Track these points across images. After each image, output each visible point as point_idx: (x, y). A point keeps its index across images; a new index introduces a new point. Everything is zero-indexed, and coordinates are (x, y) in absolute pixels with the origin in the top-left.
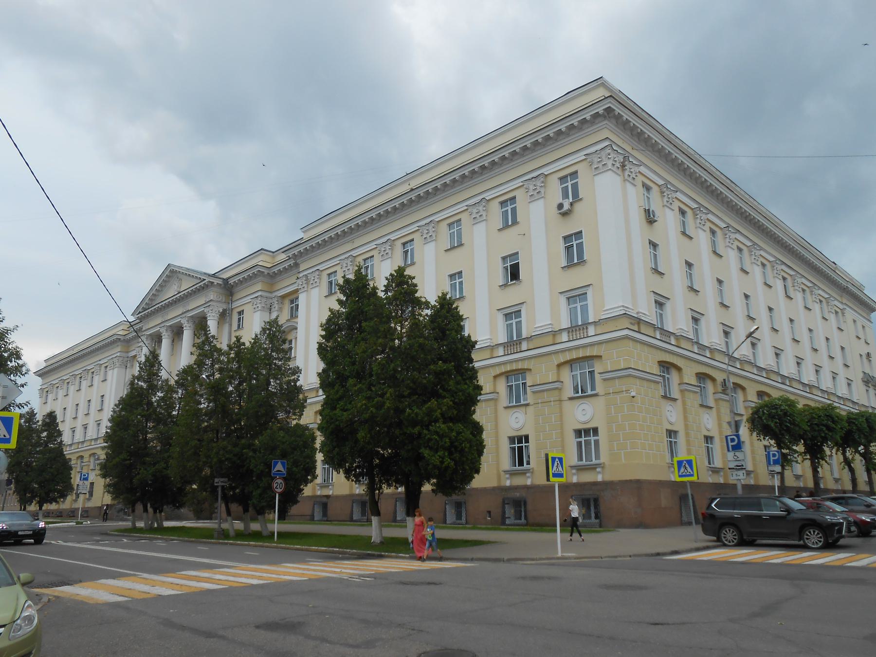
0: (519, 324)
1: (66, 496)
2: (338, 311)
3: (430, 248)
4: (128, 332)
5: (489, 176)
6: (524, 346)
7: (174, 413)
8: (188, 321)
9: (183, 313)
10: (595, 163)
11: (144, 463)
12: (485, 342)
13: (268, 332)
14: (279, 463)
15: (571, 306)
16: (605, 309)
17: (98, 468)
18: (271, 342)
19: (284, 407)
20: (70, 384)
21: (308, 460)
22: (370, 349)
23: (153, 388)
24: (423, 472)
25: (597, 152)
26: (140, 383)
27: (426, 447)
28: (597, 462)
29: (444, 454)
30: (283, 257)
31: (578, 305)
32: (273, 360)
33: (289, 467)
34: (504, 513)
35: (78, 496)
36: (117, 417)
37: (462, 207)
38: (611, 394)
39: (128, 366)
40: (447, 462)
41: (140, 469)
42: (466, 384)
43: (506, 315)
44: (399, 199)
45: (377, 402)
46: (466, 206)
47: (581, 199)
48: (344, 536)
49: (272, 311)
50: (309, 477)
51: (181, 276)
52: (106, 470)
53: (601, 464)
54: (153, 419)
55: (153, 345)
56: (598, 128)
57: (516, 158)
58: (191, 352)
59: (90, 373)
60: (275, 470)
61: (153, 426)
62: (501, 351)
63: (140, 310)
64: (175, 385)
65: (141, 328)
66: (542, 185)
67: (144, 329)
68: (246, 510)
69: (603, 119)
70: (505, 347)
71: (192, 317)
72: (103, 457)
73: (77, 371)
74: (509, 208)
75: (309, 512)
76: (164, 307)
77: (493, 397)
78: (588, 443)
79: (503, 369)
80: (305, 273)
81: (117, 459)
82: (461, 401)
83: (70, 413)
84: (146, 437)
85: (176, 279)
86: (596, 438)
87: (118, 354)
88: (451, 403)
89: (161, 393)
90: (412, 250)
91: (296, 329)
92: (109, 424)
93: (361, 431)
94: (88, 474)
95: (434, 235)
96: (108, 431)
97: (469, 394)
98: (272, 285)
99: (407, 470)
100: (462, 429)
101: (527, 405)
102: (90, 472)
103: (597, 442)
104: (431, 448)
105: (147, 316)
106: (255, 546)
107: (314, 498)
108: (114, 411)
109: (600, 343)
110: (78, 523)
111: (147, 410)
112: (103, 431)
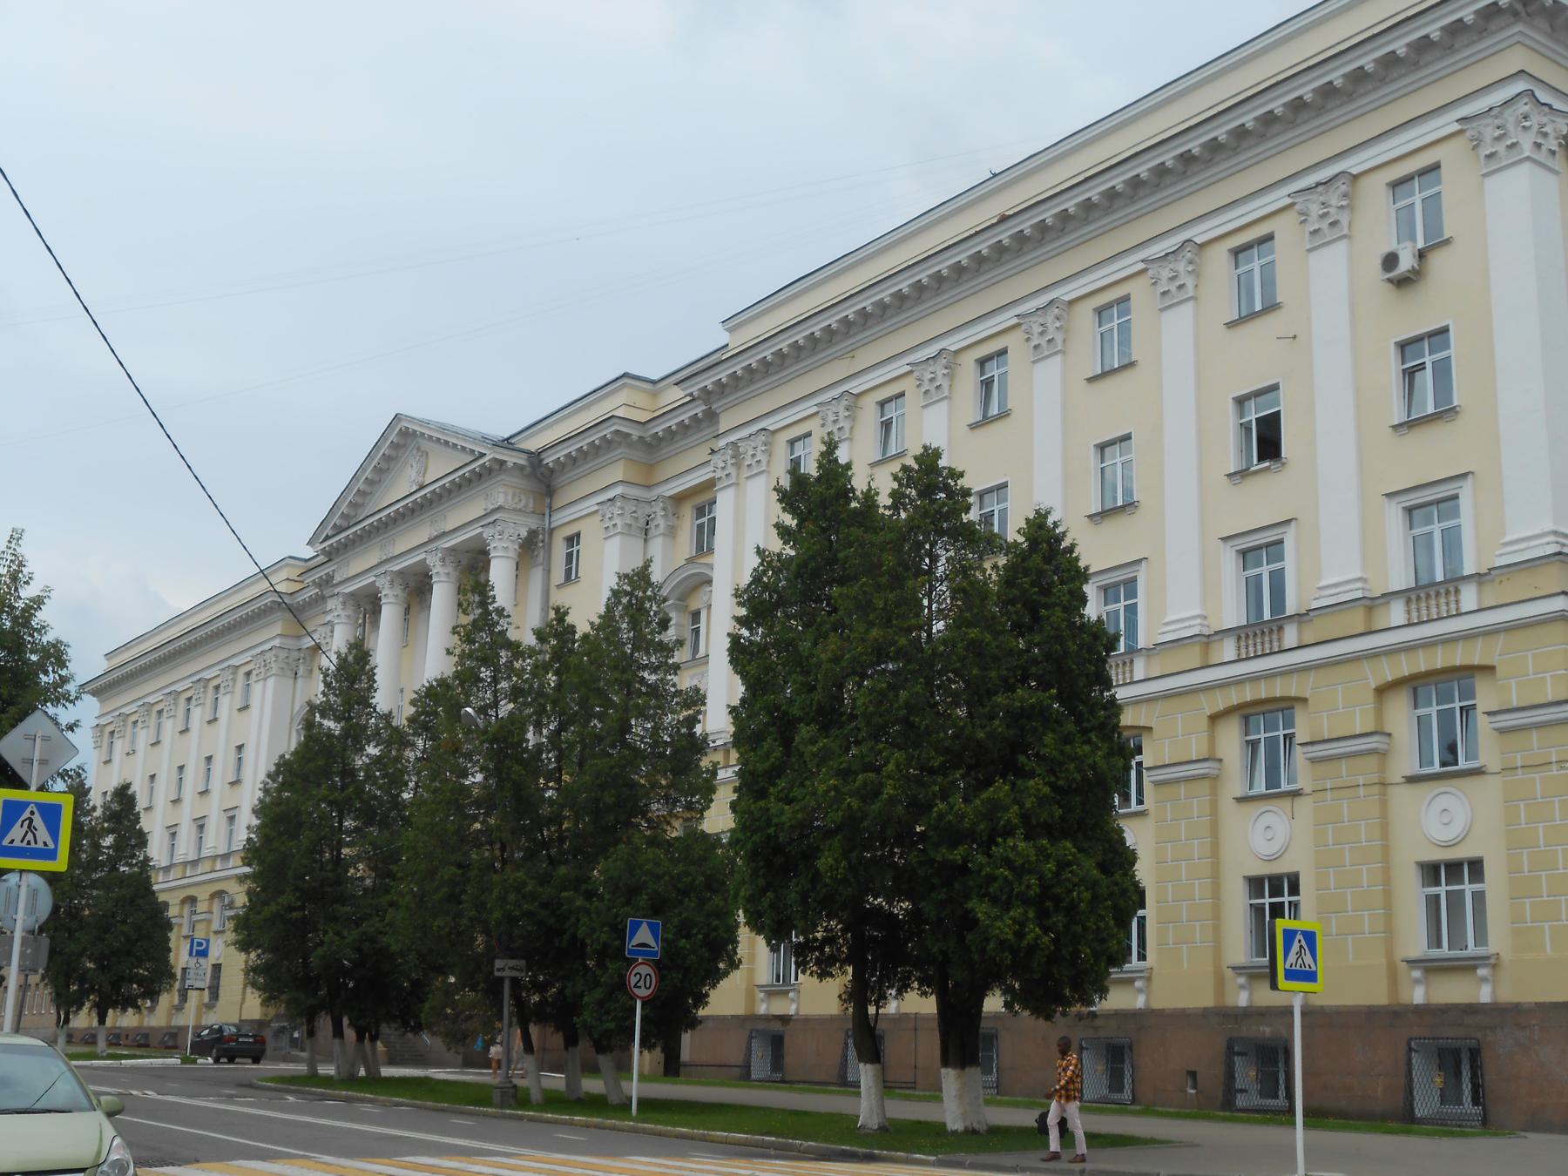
0: (1278, 580)
1: (158, 993)
2: (779, 555)
3: (1049, 372)
4: (299, 586)
5: (879, 331)
6: (1290, 636)
7: (405, 796)
8: (443, 560)
9: (431, 541)
10: (1164, 280)
11: (335, 918)
12: (1187, 624)
13: (625, 600)
14: (644, 925)
15: (1417, 531)
16: (1507, 539)
17: (230, 925)
18: (634, 625)
19: (661, 787)
20: (165, 714)
21: (715, 923)
22: (849, 652)
23: (355, 736)
24: (976, 957)
25: (1494, 112)
26: (326, 722)
27: (981, 896)
28: (1481, 951)
29: (1026, 913)
30: (675, 395)
31: (1436, 529)
32: (639, 668)
33: (670, 936)
34: (1230, 1076)
35: (184, 996)
36: (272, 803)
37: (1132, 263)
38: (1519, 770)
39: (300, 673)
40: (1033, 935)
41: (326, 932)
42: (1089, 742)
43: (1244, 553)
44: (890, 282)
45: (865, 784)
46: (1289, 196)
47: (1447, 242)
48: (805, 1113)
49: (651, 534)
50: (721, 965)
51: (424, 444)
52: (248, 932)
53: (1487, 958)
54: (356, 811)
55: (360, 621)
56: (1114, 221)
57: (1305, 115)
58: (448, 650)
59: (210, 689)
60: (635, 941)
61: (355, 827)
62: (1228, 650)
63: (329, 531)
64: (409, 726)
65: (330, 577)
66: (1344, 203)
67: (337, 579)
68: (571, 1041)
69: (1512, 19)
70: (1239, 638)
71: (452, 550)
72: (241, 899)
73: (208, 671)
74: (1256, 266)
75: (737, 1057)
76: (386, 524)
77: (1206, 771)
78: (1455, 900)
79: (1234, 697)
80: (733, 438)
81: (273, 908)
82: (1074, 786)
83: (164, 791)
84: (339, 853)
85: (415, 452)
86: (1477, 887)
87: (277, 642)
88: (1046, 790)
89: (375, 747)
90: (1003, 376)
91: (709, 582)
92: (256, 822)
93: (826, 853)
94: (208, 941)
95: (1059, 339)
96: (253, 836)
97: (1094, 767)
98: (651, 467)
99: (935, 950)
100: (1073, 855)
101: (1296, 794)
102: (212, 938)
103: (1479, 898)
104: (994, 900)
105: (413, 511)
106: (587, 1126)
107: (751, 1025)
108: (266, 791)
109: (1490, 632)
110: (185, 1061)
111: (343, 789)
112: (242, 835)
